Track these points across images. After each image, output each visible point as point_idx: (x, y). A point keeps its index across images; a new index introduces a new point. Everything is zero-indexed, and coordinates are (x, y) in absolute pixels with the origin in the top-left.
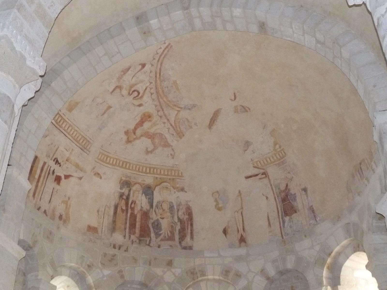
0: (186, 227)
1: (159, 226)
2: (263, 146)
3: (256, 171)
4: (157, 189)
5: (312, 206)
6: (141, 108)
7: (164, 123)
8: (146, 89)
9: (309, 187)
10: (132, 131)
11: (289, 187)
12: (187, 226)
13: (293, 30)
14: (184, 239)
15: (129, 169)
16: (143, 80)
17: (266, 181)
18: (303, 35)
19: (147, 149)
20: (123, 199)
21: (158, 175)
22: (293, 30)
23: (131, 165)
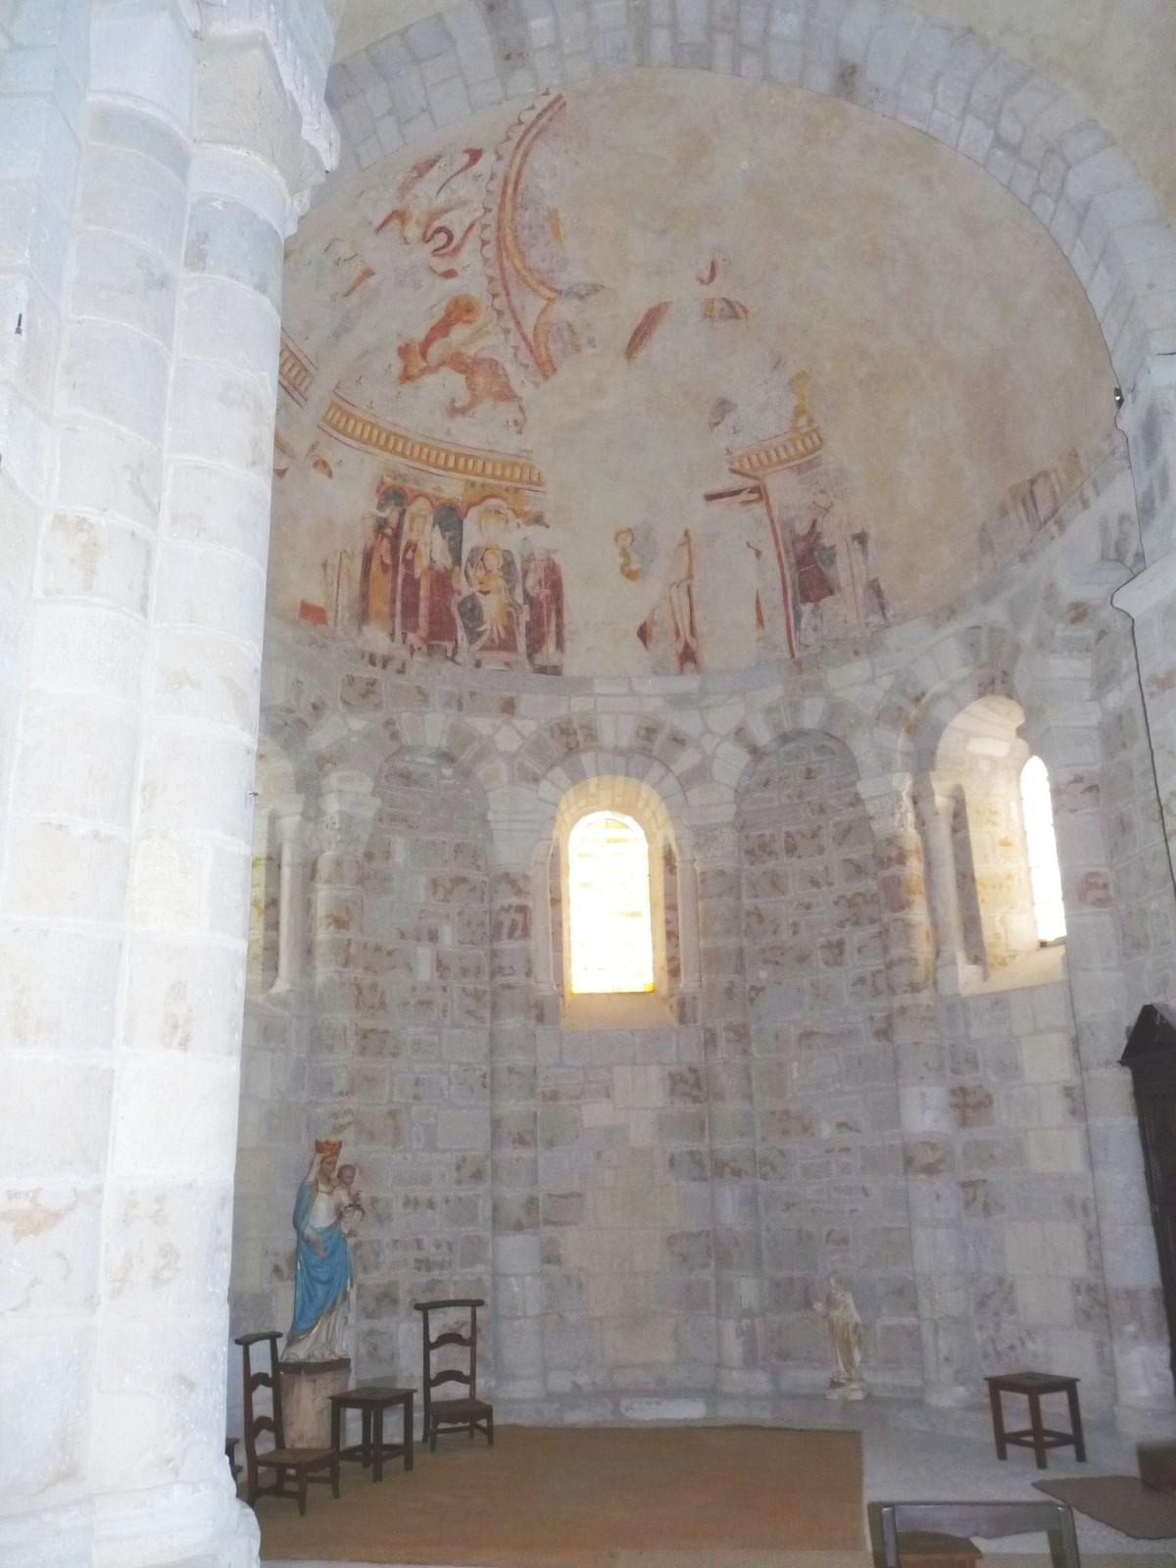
0: (545, 618)
1: (477, 612)
2: (763, 415)
3: (737, 482)
4: (473, 513)
6: (451, 283)
7: (507, 331)
8: (471, 227)
9: (873, 532)
10: (417, 349)
11: (818, 529)
12: (548, 616)
13: (935, 99)
14: (540, 647)
15: (403, 455)
16: (467, 199)
17: (759, 509)
18: (962, 118)
19: (453, 401)
20: (384, 535)
21: (475, 474)
22: (935, 99)
23: (410, 445)
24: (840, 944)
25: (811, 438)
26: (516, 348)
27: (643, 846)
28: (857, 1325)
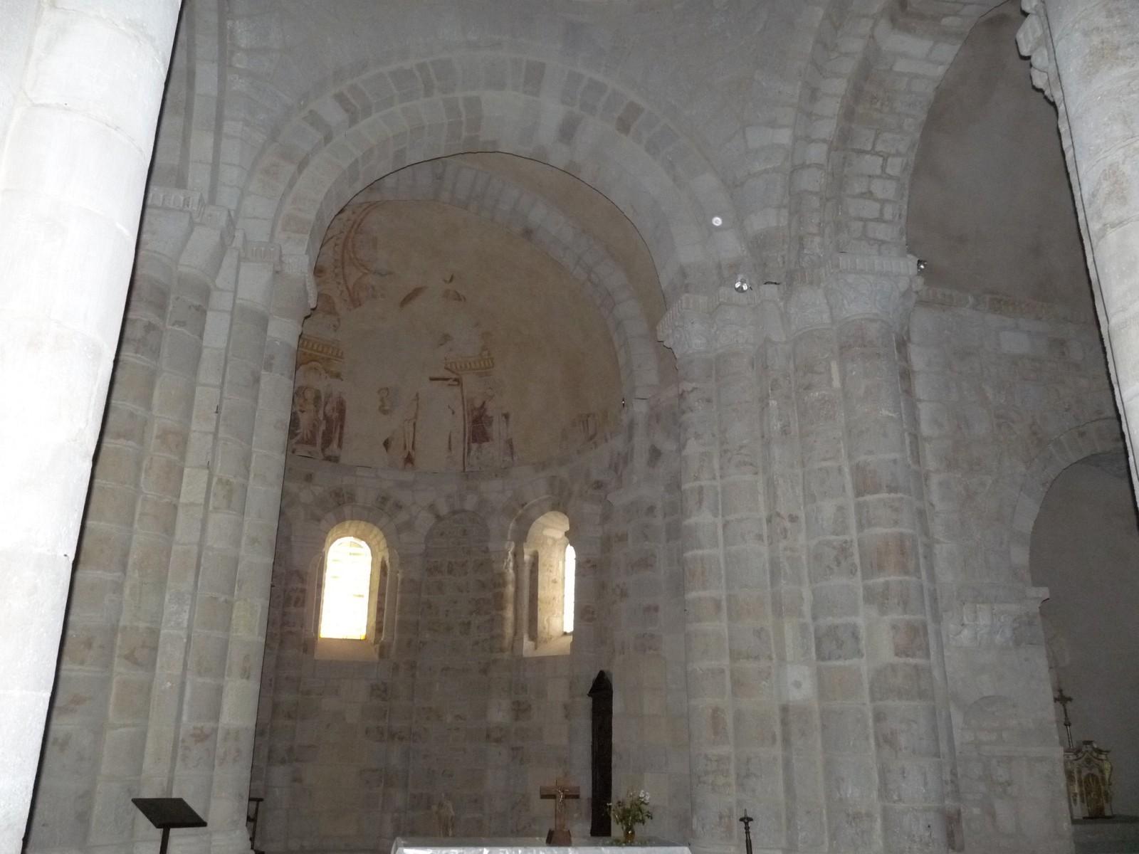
3: (447, 374)
5: (511, 439)
8: (332, 238)
12: (335, 428)
17: (456, 390)
24: (469, 623)
25: (488, 362)
26: (342, 291)
27: (369, 558)
28: (452, 817)
